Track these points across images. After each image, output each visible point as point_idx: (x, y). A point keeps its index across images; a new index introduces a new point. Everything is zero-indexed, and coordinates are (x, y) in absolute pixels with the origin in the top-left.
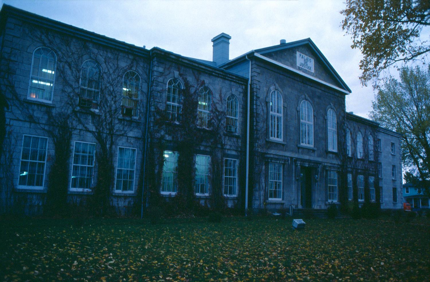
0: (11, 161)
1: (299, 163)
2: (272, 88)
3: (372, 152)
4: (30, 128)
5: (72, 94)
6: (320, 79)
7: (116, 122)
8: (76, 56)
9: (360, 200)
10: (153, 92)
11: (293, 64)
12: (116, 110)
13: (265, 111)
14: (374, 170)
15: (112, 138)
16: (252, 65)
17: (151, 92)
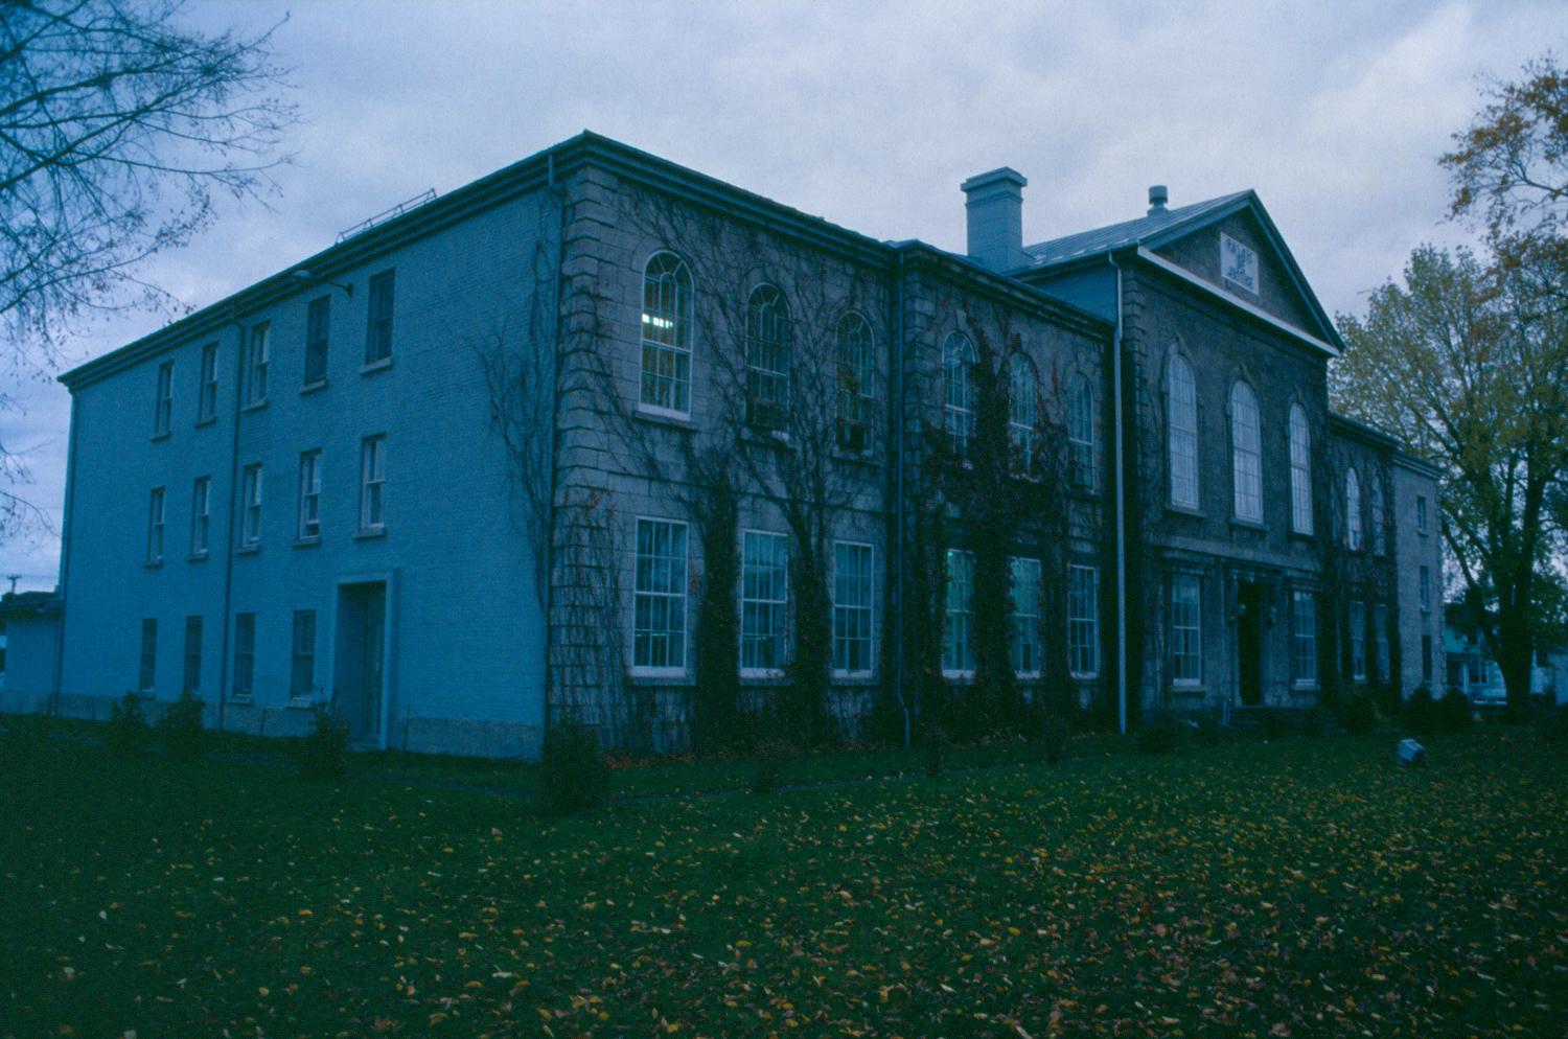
0: (617, 597)
1: (1235, 573)
2: (1173, 348)
3: (1379, 529)
4: (650, 496)
5: (731, 391)
6: (1271, 312)
7: (828, 467)
8: (734, 275)
9: (1021, 675)
10: (917, 376)
11: (1213, 274)
12: (825, 433)
13: (1160, 421)
14: (1386, 584)
15: (820, 516)
16: (1124, 280)
17: (907, 376)
